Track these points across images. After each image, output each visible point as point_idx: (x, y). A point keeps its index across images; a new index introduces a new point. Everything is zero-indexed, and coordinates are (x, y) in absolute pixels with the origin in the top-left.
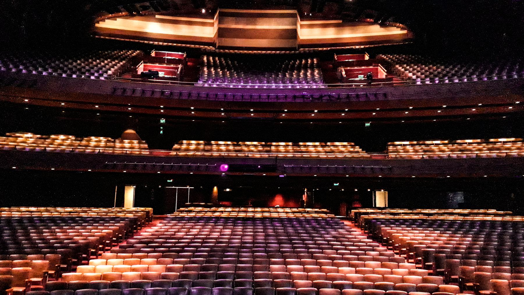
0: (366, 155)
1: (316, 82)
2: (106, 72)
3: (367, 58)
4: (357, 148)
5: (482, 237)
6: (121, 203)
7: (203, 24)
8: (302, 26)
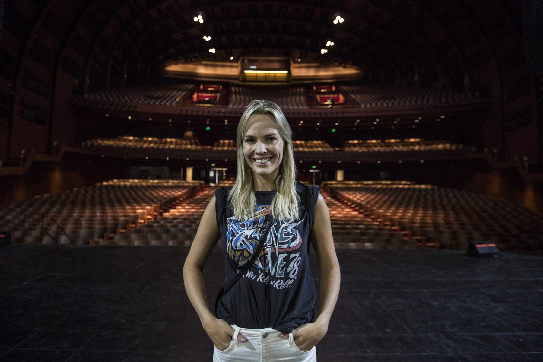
0: (331, 150)
1: (302, 104)
2: (175, 100)
3: (334, 88)
4: (327, 145)
5: (394, 196)
6: (185, 178)
7: (232, 67)
8: (294, 67)
